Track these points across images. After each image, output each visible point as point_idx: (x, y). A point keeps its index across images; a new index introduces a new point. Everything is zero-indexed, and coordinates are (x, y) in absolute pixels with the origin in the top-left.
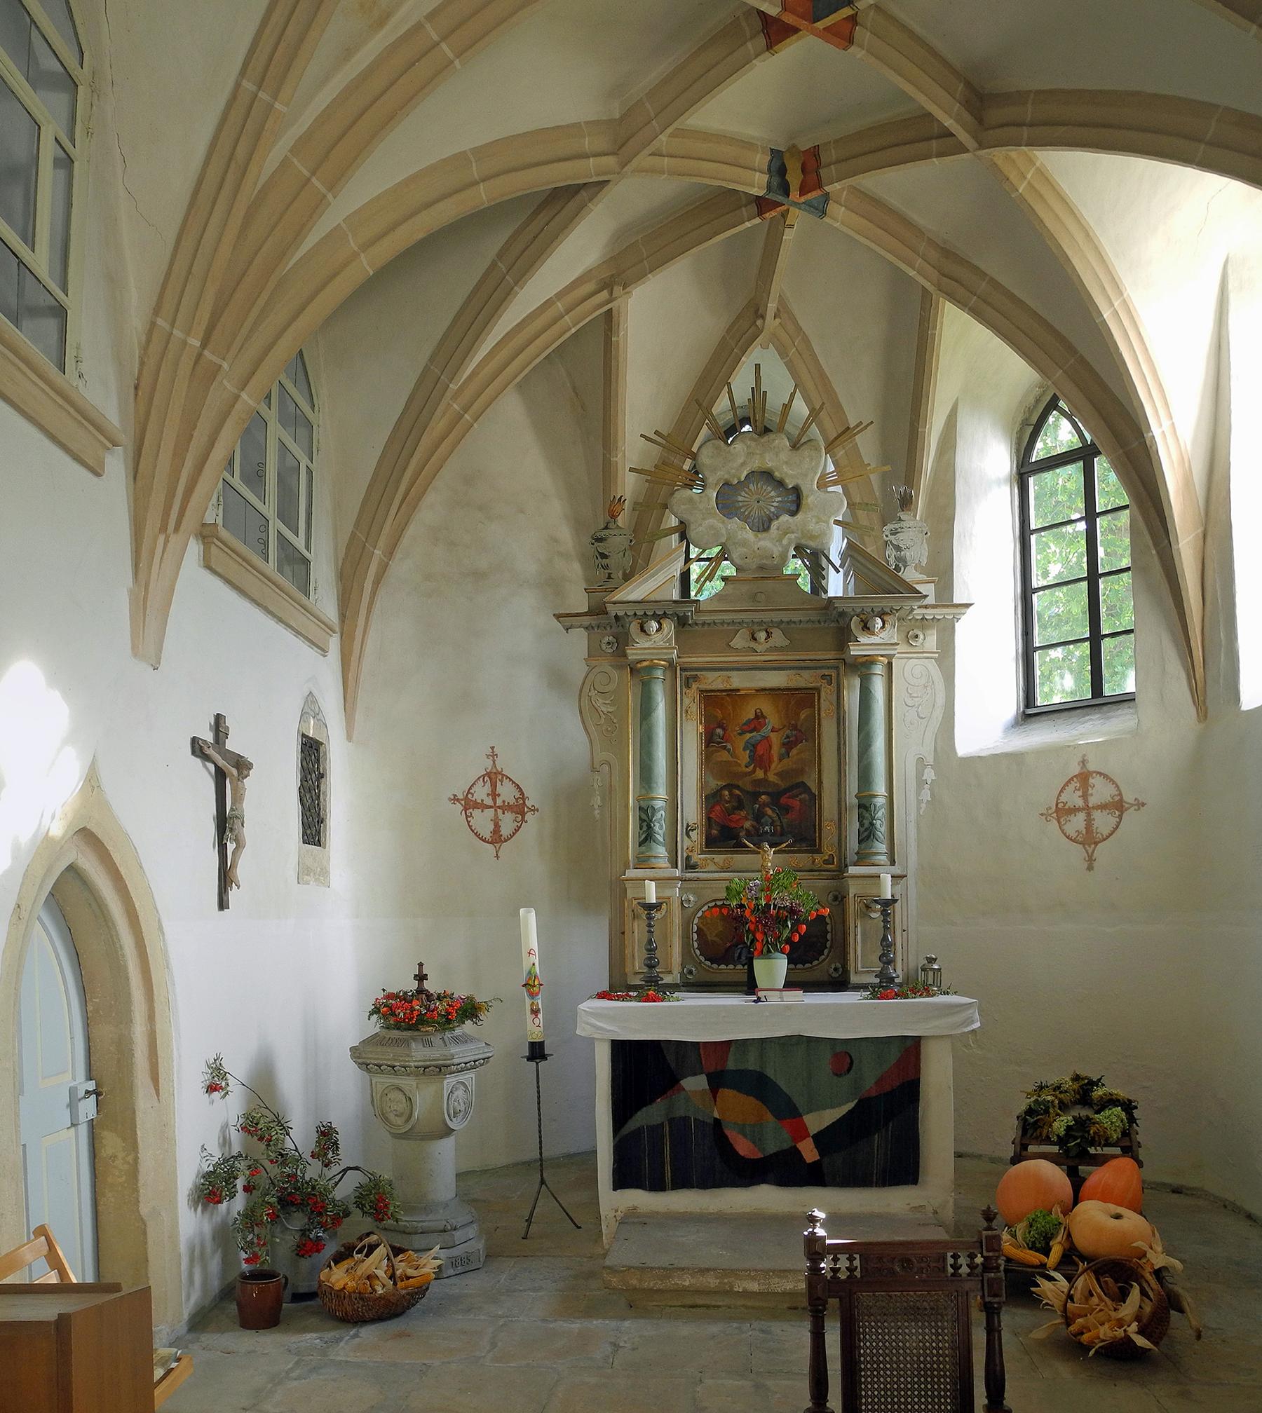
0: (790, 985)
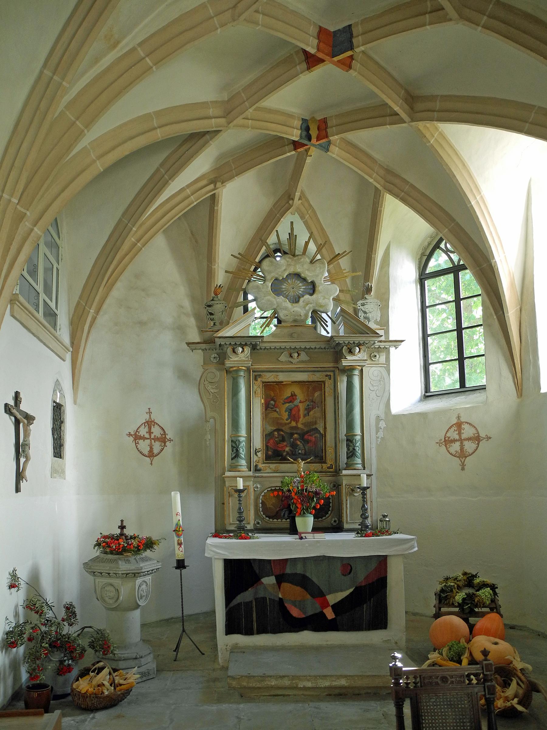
0: (315, 530)
